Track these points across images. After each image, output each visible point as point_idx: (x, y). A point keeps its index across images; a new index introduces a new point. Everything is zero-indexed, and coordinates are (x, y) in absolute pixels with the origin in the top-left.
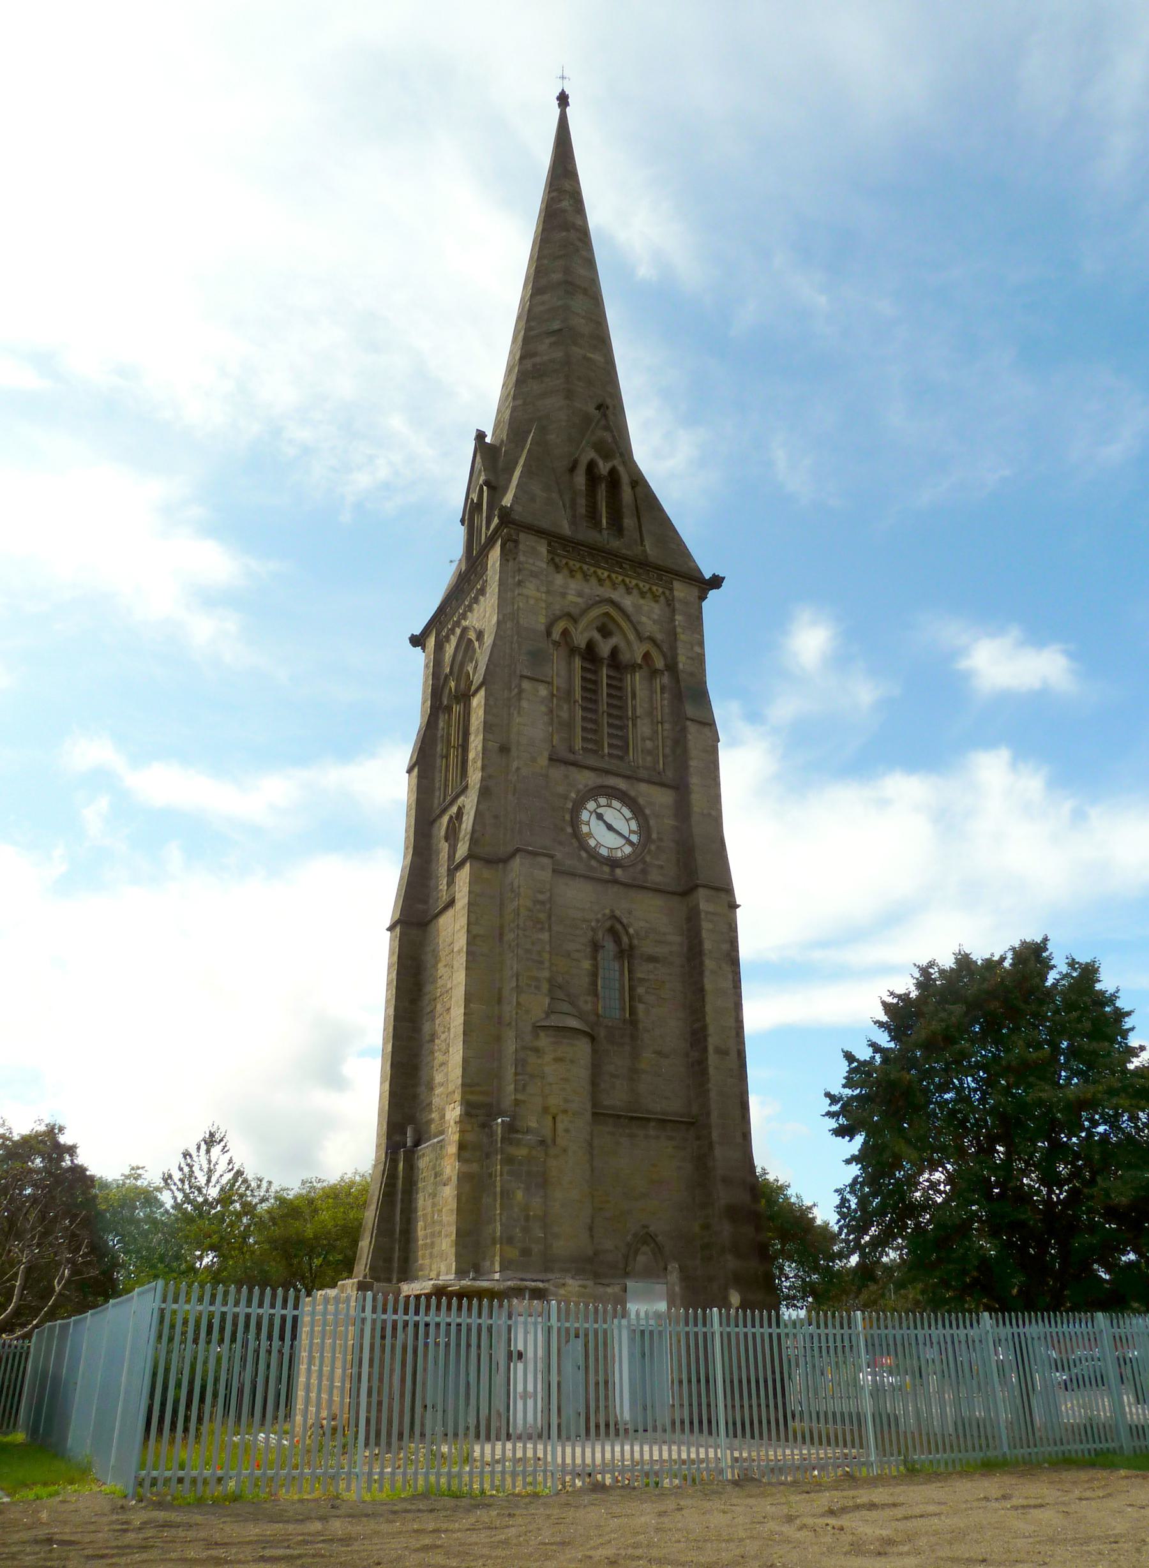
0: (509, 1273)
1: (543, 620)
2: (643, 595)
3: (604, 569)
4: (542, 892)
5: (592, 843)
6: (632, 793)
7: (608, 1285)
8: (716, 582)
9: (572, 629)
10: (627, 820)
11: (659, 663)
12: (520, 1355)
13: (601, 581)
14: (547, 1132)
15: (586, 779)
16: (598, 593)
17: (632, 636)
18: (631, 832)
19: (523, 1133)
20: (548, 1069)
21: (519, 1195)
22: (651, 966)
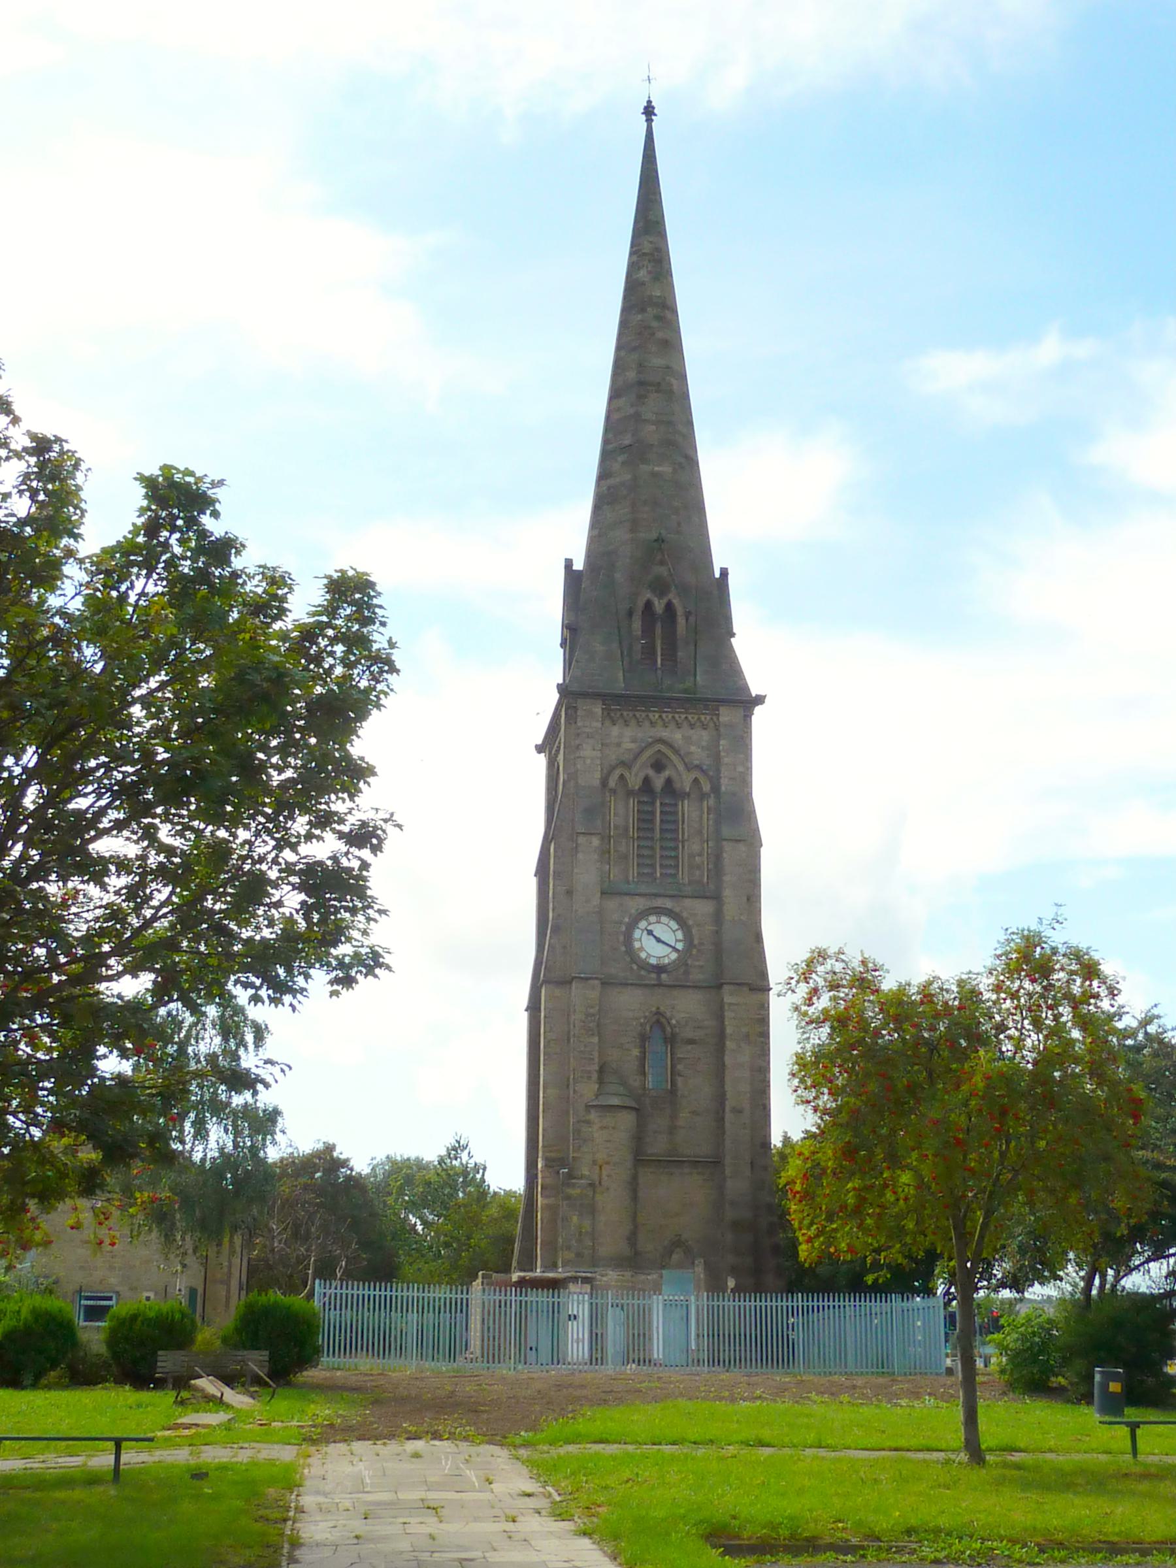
0: (568, 1268)
1: (598, 775)
2: (692, 726)
3: (654, 711)
4: (592, 1007)
5: (643, 955)
6: (677, 910)
7: (649, 1274)
8: (760, 700)
9: (627, 775)
10: (674, 931)
11: (706, 787)
12: (575, 1317)
13: (653, 724)
14: (596, 1178)
15: (640, 903)
16: (651, 734)
17: (681, 767)
18: (677, 941)
19: (578, 1179)
20: (596, 1135)
21: (575, 1219)
22: (689, 1047)
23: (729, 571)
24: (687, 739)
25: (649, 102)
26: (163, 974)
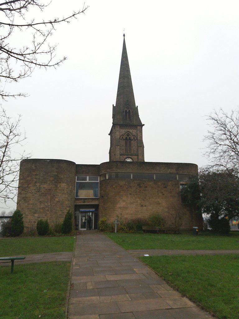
8: (144, 125)
11: (136, 139)
13: (127, 129)
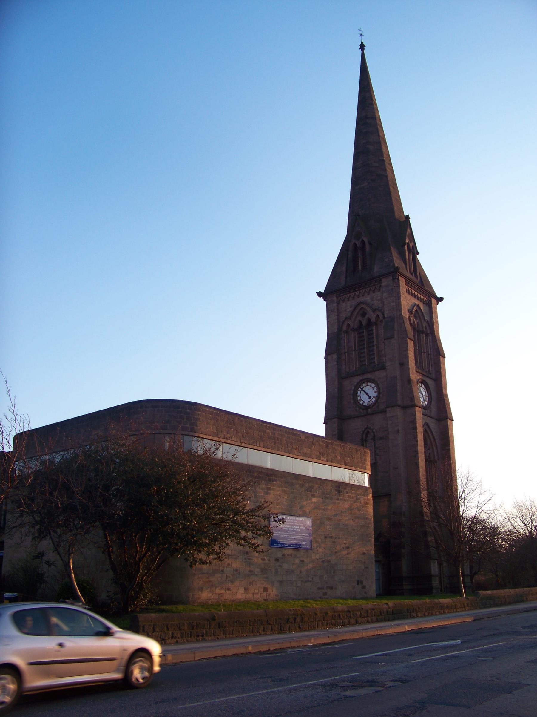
10: (373, 388)
23: (444, 299)
24: (372, 299)
25: (362, 43)
26: (477, 545)
